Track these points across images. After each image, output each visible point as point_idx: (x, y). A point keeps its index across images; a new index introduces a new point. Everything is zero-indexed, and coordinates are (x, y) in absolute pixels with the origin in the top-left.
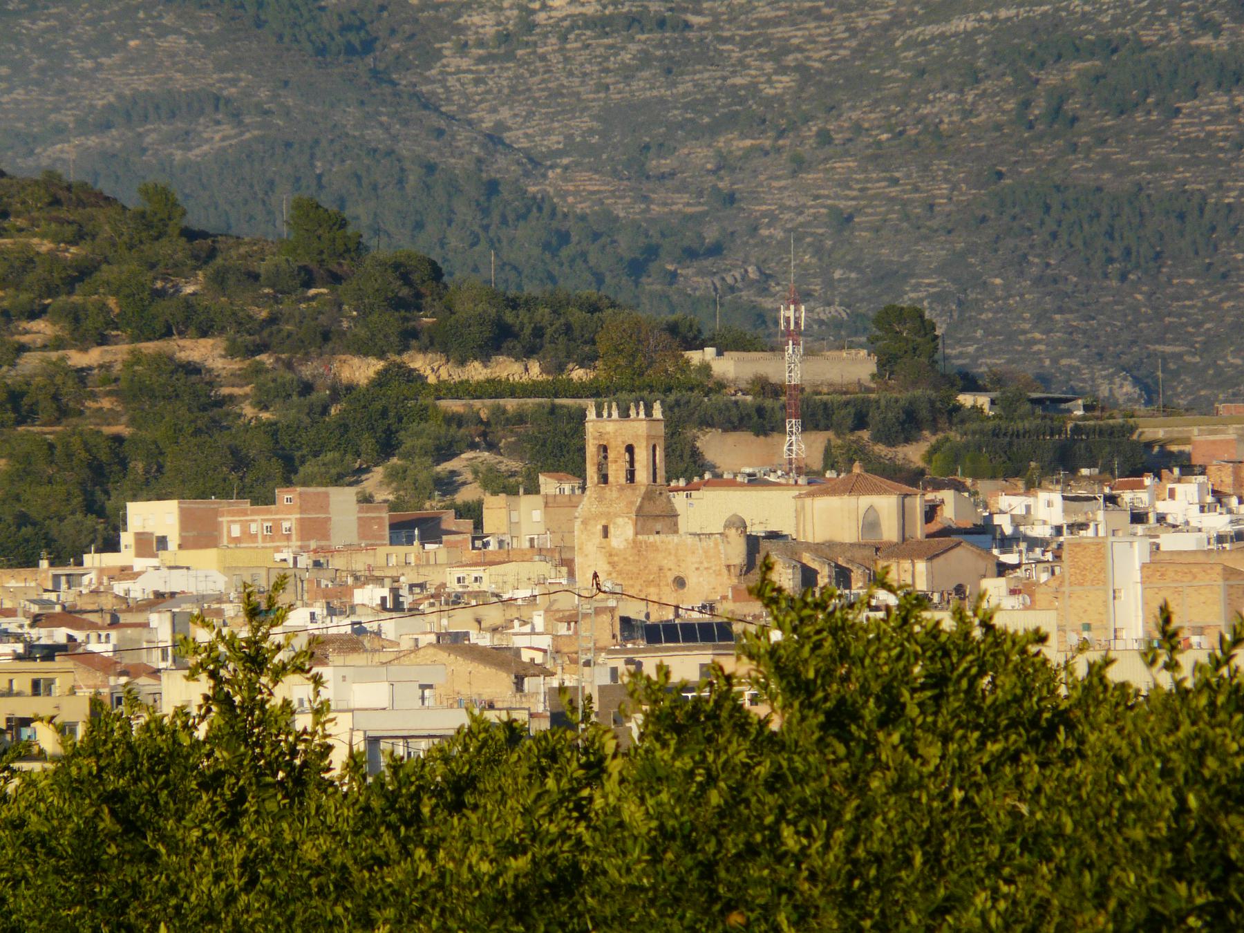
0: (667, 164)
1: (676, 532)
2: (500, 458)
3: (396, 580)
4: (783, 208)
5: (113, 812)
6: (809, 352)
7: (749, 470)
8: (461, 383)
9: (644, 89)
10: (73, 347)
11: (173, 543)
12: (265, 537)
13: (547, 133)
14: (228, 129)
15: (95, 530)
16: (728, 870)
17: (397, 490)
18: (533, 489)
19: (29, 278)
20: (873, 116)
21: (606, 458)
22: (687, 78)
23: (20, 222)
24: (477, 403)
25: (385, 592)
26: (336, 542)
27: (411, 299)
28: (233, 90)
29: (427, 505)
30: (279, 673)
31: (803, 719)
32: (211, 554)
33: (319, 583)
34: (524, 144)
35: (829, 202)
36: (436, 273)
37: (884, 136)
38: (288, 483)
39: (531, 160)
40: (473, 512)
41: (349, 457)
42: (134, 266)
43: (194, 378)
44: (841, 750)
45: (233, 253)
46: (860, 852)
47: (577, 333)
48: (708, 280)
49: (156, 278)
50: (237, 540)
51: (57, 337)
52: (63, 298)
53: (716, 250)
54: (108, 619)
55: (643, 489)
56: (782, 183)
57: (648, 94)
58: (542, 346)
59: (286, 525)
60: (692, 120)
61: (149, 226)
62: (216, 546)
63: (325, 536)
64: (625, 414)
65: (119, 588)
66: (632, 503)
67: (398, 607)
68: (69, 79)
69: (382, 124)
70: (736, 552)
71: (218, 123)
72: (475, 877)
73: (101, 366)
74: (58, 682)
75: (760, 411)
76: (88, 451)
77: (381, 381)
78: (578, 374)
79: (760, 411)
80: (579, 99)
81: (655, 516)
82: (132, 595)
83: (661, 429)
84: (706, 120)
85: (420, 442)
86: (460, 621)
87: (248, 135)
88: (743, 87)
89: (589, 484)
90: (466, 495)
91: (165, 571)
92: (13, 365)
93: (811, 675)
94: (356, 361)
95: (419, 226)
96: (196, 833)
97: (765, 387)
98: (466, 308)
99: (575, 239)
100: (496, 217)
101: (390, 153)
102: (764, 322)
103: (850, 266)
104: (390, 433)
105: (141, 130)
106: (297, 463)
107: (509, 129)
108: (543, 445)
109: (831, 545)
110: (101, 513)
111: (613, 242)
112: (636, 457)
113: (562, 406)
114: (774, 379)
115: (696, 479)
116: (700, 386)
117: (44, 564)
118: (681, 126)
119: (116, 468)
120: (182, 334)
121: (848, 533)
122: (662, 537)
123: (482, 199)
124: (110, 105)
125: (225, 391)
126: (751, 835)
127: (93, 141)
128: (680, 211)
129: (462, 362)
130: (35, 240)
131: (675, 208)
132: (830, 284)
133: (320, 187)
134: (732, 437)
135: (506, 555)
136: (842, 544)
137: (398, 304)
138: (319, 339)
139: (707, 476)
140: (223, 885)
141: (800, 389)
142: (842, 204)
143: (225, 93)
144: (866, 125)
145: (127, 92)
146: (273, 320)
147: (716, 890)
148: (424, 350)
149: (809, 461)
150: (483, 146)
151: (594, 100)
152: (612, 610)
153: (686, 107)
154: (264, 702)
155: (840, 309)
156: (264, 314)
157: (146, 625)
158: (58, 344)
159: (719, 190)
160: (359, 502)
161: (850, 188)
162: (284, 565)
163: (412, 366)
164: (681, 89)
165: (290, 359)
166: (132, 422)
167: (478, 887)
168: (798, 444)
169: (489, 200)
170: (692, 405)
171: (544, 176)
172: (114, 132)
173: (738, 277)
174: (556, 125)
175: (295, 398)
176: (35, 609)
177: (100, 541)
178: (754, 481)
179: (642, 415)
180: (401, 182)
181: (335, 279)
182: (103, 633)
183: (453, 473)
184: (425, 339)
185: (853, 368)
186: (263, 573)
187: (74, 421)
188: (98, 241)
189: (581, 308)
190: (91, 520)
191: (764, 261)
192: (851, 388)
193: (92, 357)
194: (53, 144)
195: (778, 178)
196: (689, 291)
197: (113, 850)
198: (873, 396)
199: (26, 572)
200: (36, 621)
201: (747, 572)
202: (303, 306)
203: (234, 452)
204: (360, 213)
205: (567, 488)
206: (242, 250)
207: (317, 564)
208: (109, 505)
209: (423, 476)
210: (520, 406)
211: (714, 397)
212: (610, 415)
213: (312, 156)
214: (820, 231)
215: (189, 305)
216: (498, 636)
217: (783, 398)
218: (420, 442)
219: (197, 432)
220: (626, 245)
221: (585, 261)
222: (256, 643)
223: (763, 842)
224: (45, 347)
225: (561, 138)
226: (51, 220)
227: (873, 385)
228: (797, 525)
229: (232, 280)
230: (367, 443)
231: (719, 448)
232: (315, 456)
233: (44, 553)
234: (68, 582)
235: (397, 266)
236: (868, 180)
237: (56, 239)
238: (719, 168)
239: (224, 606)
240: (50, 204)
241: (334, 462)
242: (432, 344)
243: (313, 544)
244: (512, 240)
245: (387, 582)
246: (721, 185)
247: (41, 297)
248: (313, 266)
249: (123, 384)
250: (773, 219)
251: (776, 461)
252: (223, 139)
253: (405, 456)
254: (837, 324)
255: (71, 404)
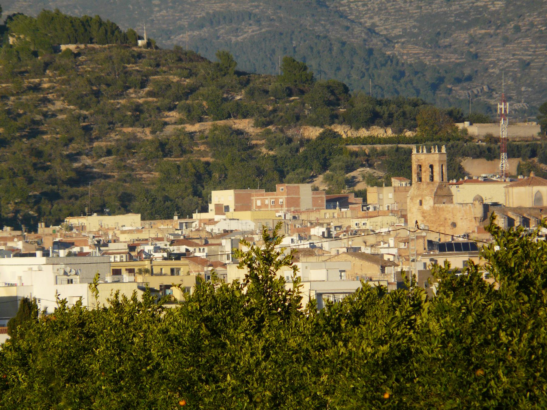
0: (448, 41)
1: (452, 203)
2: (374, 171)
3: (329, 224)
4: (499, 60)
5: (206, 326)
6: (510, 124)
7: (484, 175)
8: (357, 138)
9: (438, 8)
10: (187, 123)
11: (232, 209)
12: (271, 206)
13: (395, 28)
14: (255, 28)
15: (198, 203)
16: (476, 351)
17: (329, 185)
18: (389, 184)
19: (169, 93)
20: (538, 19)
21: (421, 170)
22: (456, 3)
23: (164, 69)
24: (364, 147)
25: (324, 230)
26: (303, 208)
27: (335, 101)
28: (257, 10)
29: (342, 192)
30: (278, 265)
31: (509, 285)
32: (248, 213)
33: (295, 226)
34: (385, 32)
35: (519, 57)
36: (346, 90)
37: (543, 28)
38: (281, 182)
39: (387, 40)
40: (363, 195)
41: (308, 171)
42: (214, 87)
43: (240, 136)
44: (526, 298)
45: (257, 81)
46: (535, 343)
47: (408, 116)
48: (466, 92)
49: (224, 93)
50: (259, 207)
51: (181, 119)
52: (183, 102)
53: (469, 79)
54: (204, 242)
55: (437, 184)
56: (499, 49)
57: (439, 10)
58: (392, 121)
59: (281, 200)
60: (458, 21)
61: (221, 70)
62: (250, 210)
63: (298, 205)
64: (429, 151)
65: (208, 228)
66: (433, 190)
67: (330, 236)
68: (186, 6)
69: (322, 24)
70: (479, 211)
71: (250, 25)
72: (364, 354)
73: (200, 131)
74: (182, 269)
75: (489, 149)
76: (195, 168)
77: (321, 137)
78: (409, 134)
79: (489, 149)
80: (408, 12)
81: (443, 196)
82: (214, 231)
83: (445, 158)
84: (465, 21)
85: (340, 163)
86: (357, 242)
87: (263, 30)
88: (481, 7)
89: (413, 182)
90: (359, 187)
91: (228, 221)
92: (162, 131)
93: (513, 265)
94: (311, 129)
95: (339, 69)
96: (243, 335)
97: (492, 139)
98: (359, 105)
99: (407, 74)
100: (372, 64)
101: (325, 37)
102: (491, 110)
103: (529, 85)
104: (326, 160)
105: (216, 28)
106: (285, 173)
107: (378, 26)
108: (393, 165)
109: (520, 208)
110: (200, 196)
111: (424, 75)
112: (434, 170)
113: (402, 148)
114: (495, 135)
115: (461, 180)
116: (463, 139)
117: (176, 218)
118: (454, 24)
119: (207, 176)
120: (235, 117)
121: (528, 203)
122: (446, 205)
123: (366, 57)
124: (204, 17)
125: (254, 142)
126: (486, 336)
127: (196, 33)
128: (453, 62)
129: (357, 129)
130: (171, 77)
131: (452, 60)
132: (520, 93)
133: (295, 52)
134: (477, 162)
135: (377, 213)
136: (525, 208)
137: (329, 103)
138: (295, 119)
139: (466, 178)
140: (254, 358)
141: (506, 139)
142: (525, 58)
143: (254, 11)
144: (536, 23)
145: (211, 11)
146: (275, 111)
147: (471, 360)
148: (341, 123)
149: (510, 171)
150: (367, 34)
151: (416, 13)
152: (424, 237)
153: (456, 15)
154: (272, 278)
155: (524, 104)
156: (271, 108)
157: (220, 244)
158: (181, 122)
159: (471, 52)
160: (312, 190)
161: (528, 51)
162: (280, 218)
163: (335, 130)
164: (453, 8)
165: (282, 128)
166: (213, 156)
167: (366, 358)
168: (505, 164)
169: (369, 57)
170: (459, 147)
171: (394, 47)
172: (205, 29)
173: (479, 90)
174: (398, 24)
175: (284, 145)
176: (172, 238)
177: (200, 207)
178: (486, 180)
179: (437, 152)
180: (331, 50)
181: (302, 92)
182: (202, 248)
183: (354, 177)
184: (341, 119)
185: (530, 130)
186: (271, 221)
187: (189, 155)
188: (198, 76)
189: (410, 104)
190: (196, 199)
191: (491, 83)
192: (529, 139)
193: (196, 127)
194: (179, 34)
195: (497, 47)
196: (457, 97)
197: (207, 342)
198: (539, 142)
199: (168, 221)
200: (172, 243)
201: (484, 220)
202: (288, 104)
203: (258, 169)
204: (312, 64)
205: (404, 184)
206: (261, 80)
207: (294, 218)
208: (204, 192)
209: (340, 179)
210: (383, 148)
211: (468, 143)
212: (423, 152)
213: (292, 39)
214: (516, 70)
215: (238, 104)
216: (373, 249)
217: (499, 144)
218: (340, 163)
219: (242, 160)
220: (429, 77)
221: (412, 84)
222: (268, 252)
223: (492, 338)
224: (175, 123)
225: (401, 30)
226: (178, 68)
227: (539, 138)
228: (506, 200)
229: (257, 93)
230: (316, 165)
231: (471, 166)
232: (294, 170)
233: (176, 213)
234: (186, 226)
235: (329, 87)
236: (536, 48)
237: (180, 75)
238: (471, 42)
239: (254, 236)
240: (178, 61)
241: (301, 173)
242: (344, 121)
243: (292, 209)
244: (379, 76)
245: (325, 225)
246: (471, 50)
247: (174, 101)
248: (292, 87)
249: (209, 139)
250: (495, 65)
251: (496, 171)
252: (253, 31)
253: (331, 170)
254: (523, 111)
255: (187, 148)
